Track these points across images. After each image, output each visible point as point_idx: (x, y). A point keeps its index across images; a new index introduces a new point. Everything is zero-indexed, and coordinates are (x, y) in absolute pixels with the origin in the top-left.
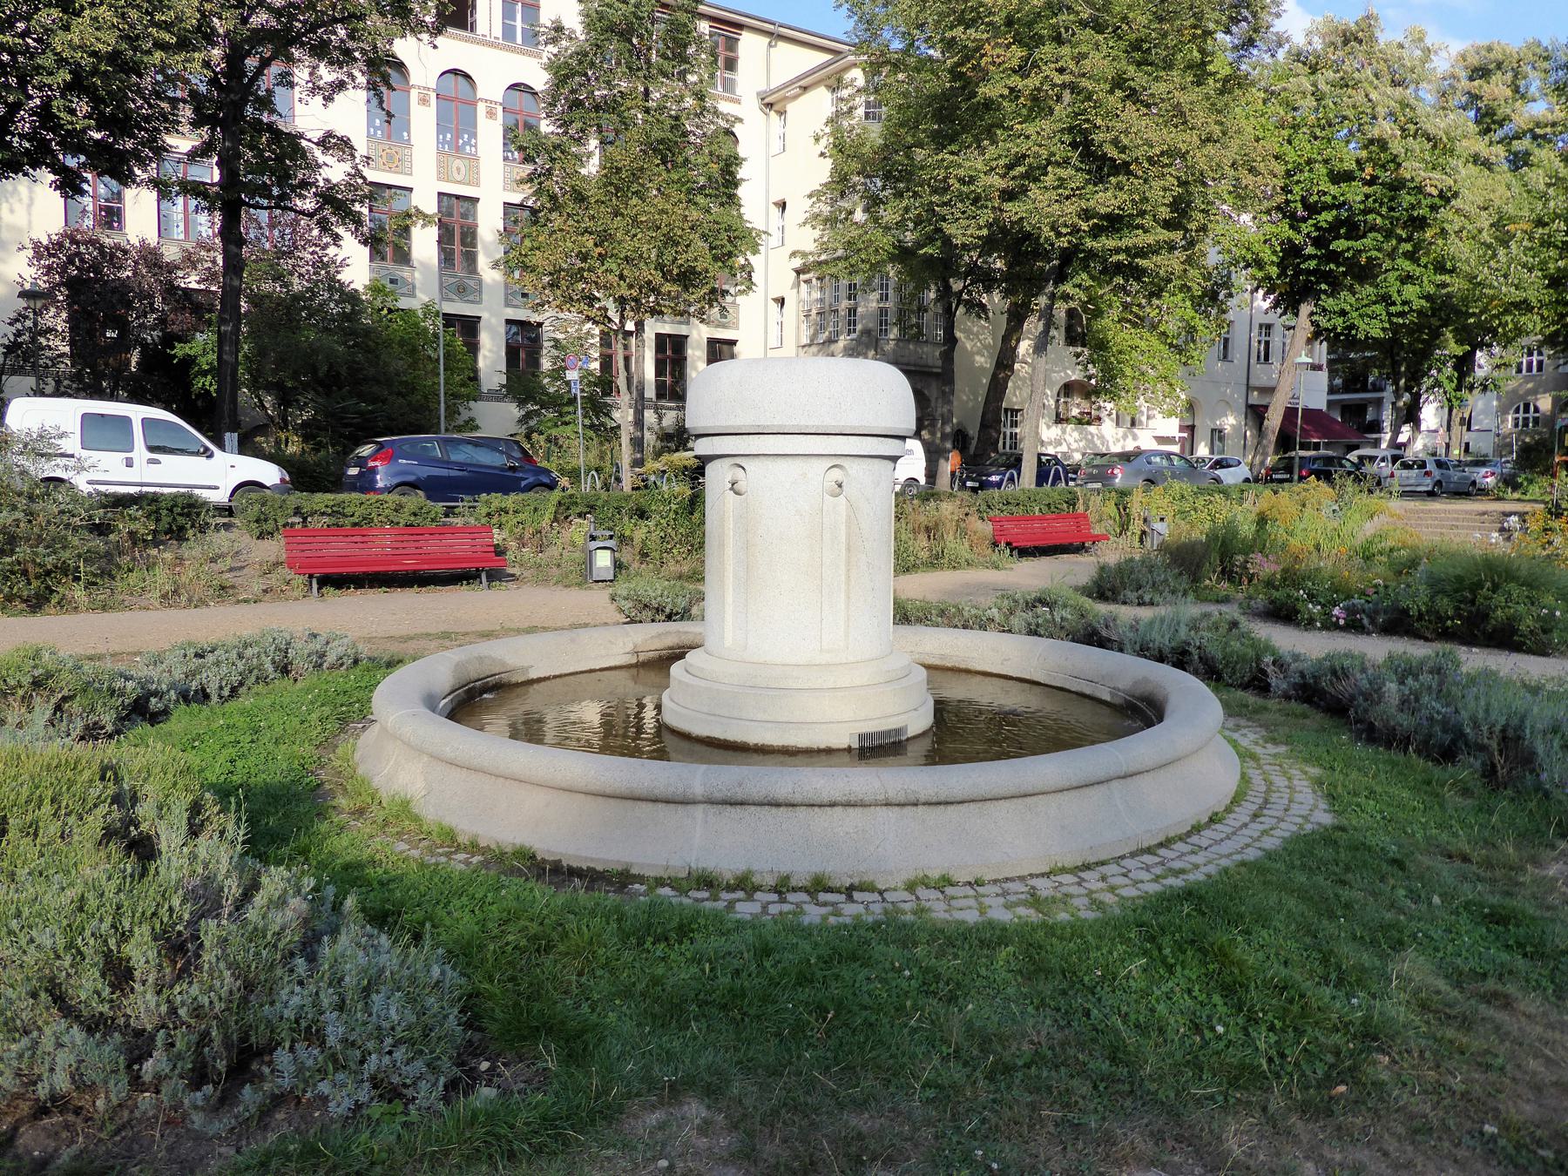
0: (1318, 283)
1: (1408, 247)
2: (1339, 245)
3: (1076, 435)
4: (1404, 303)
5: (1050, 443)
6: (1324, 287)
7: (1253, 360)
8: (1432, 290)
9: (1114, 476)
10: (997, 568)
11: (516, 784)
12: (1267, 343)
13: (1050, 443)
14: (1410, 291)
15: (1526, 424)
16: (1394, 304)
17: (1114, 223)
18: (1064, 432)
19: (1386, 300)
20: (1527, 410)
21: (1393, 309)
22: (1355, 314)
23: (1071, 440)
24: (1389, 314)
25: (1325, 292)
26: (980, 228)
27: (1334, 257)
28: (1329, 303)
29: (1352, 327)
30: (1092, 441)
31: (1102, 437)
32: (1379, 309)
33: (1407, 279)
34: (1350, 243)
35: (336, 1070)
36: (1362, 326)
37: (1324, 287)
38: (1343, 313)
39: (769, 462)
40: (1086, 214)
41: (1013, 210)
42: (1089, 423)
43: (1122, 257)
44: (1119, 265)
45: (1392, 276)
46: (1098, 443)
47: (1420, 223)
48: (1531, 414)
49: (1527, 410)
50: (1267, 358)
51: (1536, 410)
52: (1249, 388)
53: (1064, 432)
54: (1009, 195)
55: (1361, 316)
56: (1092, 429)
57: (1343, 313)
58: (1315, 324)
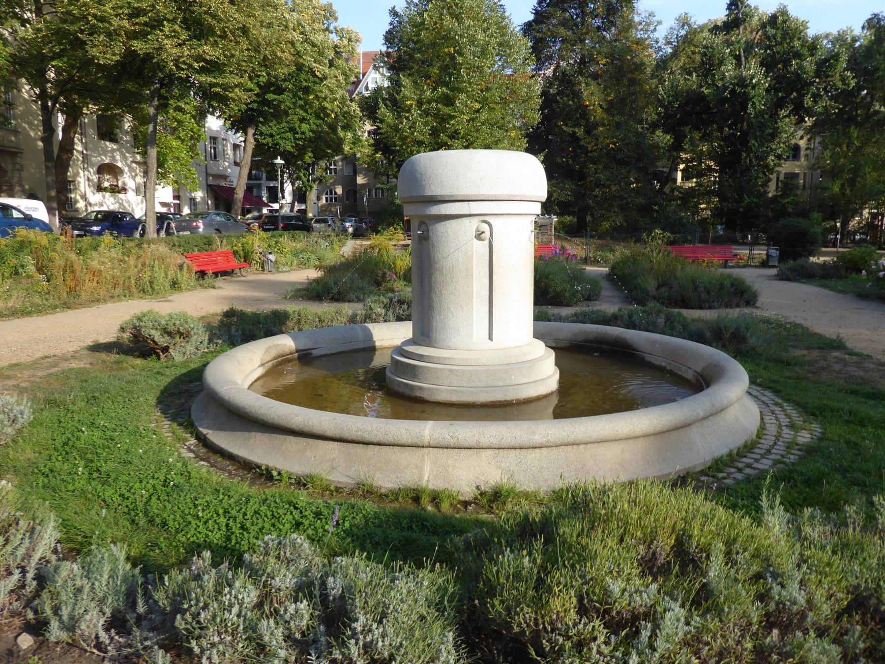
0: (258, 117)
1: (301, 102)
2: (270, 96)
3: (112, 199)
4: (303, 133)
5: (96, 205)
6: (261, 119)
7: (208, 158)
8: (314, 127)
9: (197, 227)
10: (214, 287)
11: (596, 445)
12: (215, 149)
13: (96, 205)
14: (305, 127)
15: (331, 201)
16: (297, 133)
17: (212, 67)
18: (104, 197)
19: (292, 130)
20: (331, 194)
21: (297, 136)
22: (278, 137)
23: (109, 203)
24: (295, 139)
25: (261, 123)
26: (114, 54)
27: (268, 103)
28: (264, 129)
29: (278, 144)
30: (121, 204)
31: (128, 202)
32: (290, 135)
33: (303, 120)
34: (276, 97)
35: (835, 641)
36: (283, 144)
37: (261, 119)
38: (271, 136)
39: (506, 218)
40: (199, 58)
41: (138, 46)
42: (119, 192)
43: (218, 89)
44: (217, 94)
45: (295, 118)
46: (126, 205)
47: (307, 90)
48: (333, 196)
49: (331, 194)
50: (215, 157)
51: (336, 193)
52: (207, 175)
53: (104, 197)
54: (132, 35)
55: (281, 138)
56: (121, 196)
57: (271, 136)
58: (255, 139)
